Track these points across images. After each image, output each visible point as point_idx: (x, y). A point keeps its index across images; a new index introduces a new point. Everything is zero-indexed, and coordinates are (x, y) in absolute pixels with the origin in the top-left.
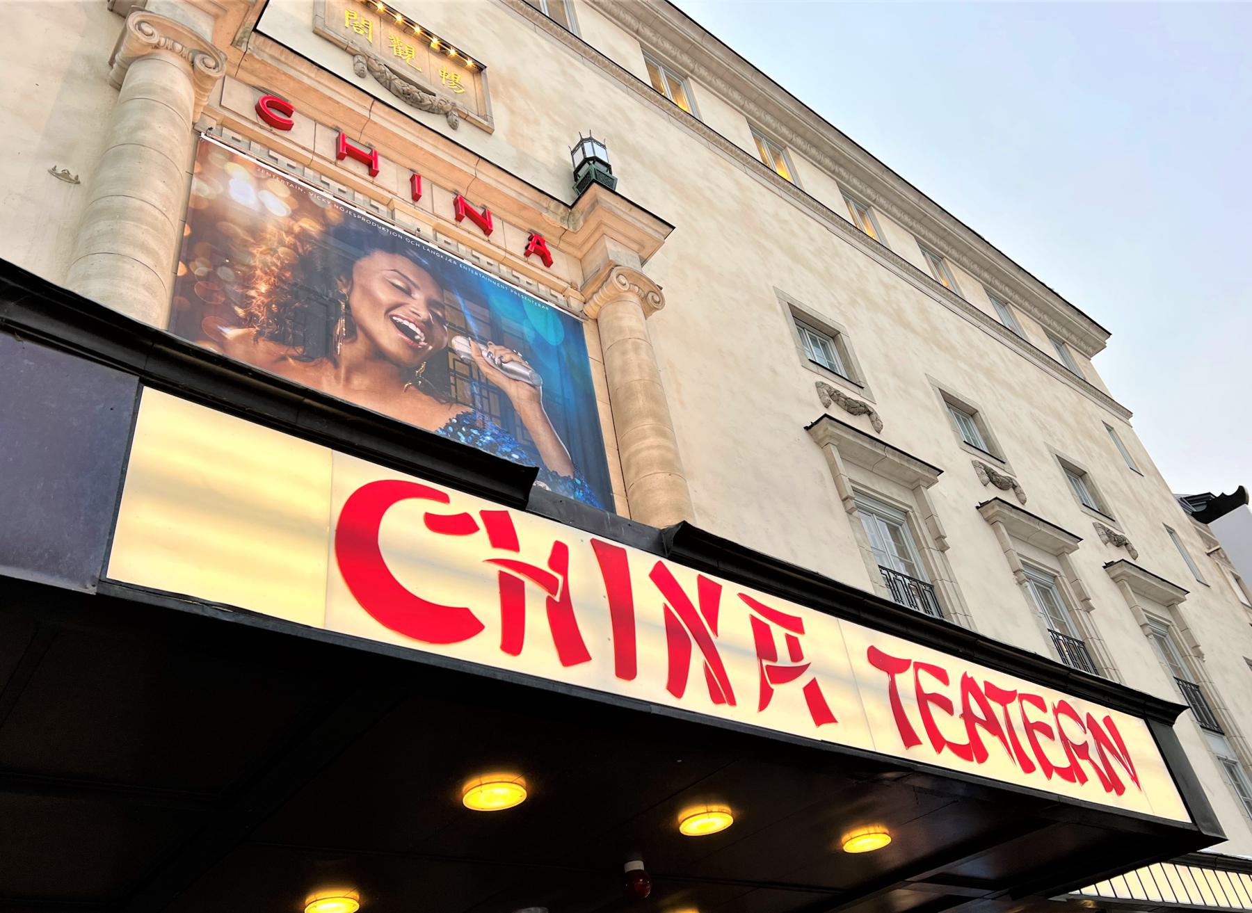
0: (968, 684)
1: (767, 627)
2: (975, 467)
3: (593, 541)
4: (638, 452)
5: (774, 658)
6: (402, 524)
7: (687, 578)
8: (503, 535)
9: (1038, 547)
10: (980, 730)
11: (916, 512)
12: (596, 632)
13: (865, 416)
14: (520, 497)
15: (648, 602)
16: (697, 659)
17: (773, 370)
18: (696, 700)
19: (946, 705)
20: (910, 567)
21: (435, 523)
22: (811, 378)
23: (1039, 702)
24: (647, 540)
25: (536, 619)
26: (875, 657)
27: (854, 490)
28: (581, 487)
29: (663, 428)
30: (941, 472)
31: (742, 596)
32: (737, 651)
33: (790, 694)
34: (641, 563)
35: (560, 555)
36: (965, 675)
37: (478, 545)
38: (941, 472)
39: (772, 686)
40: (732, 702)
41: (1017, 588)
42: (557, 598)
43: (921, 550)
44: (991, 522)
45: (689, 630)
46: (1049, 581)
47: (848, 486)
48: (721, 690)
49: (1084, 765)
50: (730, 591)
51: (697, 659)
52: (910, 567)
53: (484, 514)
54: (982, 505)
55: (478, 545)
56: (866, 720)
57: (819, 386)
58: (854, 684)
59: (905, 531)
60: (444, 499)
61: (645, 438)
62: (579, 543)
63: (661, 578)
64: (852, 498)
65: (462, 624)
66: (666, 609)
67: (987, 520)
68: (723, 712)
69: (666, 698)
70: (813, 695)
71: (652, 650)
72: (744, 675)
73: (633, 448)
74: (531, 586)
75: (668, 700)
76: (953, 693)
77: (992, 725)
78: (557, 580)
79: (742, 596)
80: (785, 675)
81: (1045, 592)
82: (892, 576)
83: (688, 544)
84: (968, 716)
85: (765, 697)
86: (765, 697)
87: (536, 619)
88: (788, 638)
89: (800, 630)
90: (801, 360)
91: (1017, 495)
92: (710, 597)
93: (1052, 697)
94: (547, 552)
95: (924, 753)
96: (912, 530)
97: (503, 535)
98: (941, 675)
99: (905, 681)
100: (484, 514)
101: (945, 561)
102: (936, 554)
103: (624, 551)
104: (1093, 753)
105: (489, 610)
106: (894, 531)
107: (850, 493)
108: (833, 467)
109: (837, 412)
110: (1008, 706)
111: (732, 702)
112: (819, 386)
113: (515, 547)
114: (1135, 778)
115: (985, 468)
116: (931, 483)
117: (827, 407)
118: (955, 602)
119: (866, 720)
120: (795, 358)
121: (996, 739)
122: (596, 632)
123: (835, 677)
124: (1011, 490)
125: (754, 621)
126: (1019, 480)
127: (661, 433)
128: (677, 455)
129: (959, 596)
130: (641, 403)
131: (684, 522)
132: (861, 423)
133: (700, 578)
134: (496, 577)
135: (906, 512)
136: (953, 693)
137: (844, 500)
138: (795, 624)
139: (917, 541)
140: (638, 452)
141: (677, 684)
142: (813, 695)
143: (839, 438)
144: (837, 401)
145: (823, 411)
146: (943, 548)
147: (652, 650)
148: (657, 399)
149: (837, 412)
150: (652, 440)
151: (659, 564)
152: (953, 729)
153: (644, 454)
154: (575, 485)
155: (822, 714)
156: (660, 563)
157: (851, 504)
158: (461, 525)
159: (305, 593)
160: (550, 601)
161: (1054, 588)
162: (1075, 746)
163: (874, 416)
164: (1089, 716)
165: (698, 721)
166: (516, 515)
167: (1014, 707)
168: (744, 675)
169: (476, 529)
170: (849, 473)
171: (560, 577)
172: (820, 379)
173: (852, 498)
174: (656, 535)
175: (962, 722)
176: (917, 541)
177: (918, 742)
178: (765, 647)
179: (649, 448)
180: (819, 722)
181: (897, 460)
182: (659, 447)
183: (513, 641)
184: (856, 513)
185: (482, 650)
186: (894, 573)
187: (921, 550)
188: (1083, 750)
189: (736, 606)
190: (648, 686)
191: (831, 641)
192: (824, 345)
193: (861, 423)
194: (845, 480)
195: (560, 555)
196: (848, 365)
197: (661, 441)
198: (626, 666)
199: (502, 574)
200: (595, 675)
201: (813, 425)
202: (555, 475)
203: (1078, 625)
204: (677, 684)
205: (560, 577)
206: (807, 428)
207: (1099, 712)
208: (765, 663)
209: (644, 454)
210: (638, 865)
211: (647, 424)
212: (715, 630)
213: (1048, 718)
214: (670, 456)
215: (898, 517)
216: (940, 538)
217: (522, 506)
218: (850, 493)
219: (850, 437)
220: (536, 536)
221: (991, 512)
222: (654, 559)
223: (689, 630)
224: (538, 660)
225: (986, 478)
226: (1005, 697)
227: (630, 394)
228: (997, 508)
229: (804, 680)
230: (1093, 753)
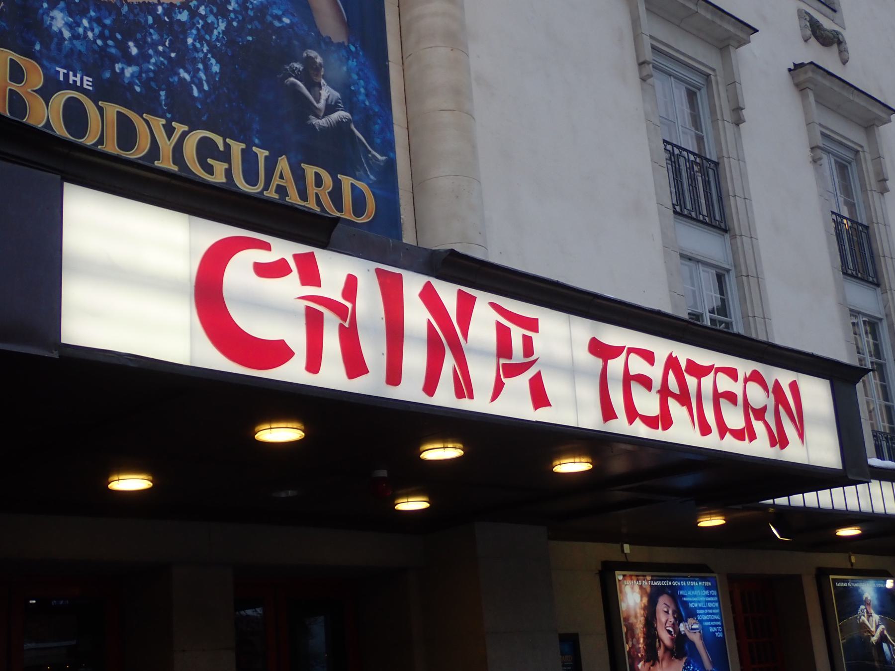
0: (672, 363)
2: (800, 17)
3: (378, 271)
5: (509, 355)
6: (239, 273)
7: (448, 294)
9: (847, 117)
10: (673, 404)
11: (719, 79)
12: (374, 351)
15: (416, 317)
19: (646, 382)
20: (700, 139)
21: (263, 270)
23: (732, 373)
25: (331, 343)
28: (355, 55)
30: (756, 31)
31: (494, 306)
32: (481, 353)
33: (520, 384)
36: (671, 354)
37: (290, 287)
38: (756, 31)
39: (504, 380)
40: (471, 397)
41: (810, 167)
42: (347, 325)
43: (714, 121)
44: (801, 88)
45: (445, 341)
46: (849, 155)
47: (647, 42)
48: (464, 388)
49: (758, 426)
51: (449, 363)
52: (700, 139)
53: (296, 257)
54: (797, 66)
56: (576, 404)
58: (572, 371)
59: (702, 98)
60: (267, 247)
62: (365, 272)
63: (429, 297)
65: (279, 352)
66: (429, 324)
67: (797, 85)
68: (465, 405)
69: (422, 398)
71: (415, 360)
72: (483, 373)
74: (328, 314)
76: (655, 373)
77: (683, 398)
80: (513, 370)
81: (843, 168)
82: (677, 151)
84: (665, 393)
86: (499, 387)
87: (331, 343)
88: (525, 337)
89: (536, 330)
91: (840, 52)
92: (466, 305)
93: (744, 367)
95: (620, 426)
96: (711, 97)
97: (310, 275)
98: (649, 357)
99: (616, 366)
100: (296, 257)
101: (738, 137)
102: (730, 127)
104: (770, 417)
106: (692, 96)
108: (635, 22)
110: (702, 379)
113: (318, 284)
114: (801, 436)
115: (811, 17)
116: (742, 43)
118: (737, 184)
119: (576, 404)
121: (685, 409)
122: (374, 351)
124: (835, 47)
125: (499, 325)
126: (848, 36)
129: (743, 175)
134: (303, 311)
135: (708, 76)
136: (655, 373)
137: (642, 64)
139: (713, 112)
141: (430, 387)
146: (738, 121)
147: (415, 360)
152: (647, 403)
154: (349, 51)
155: (540, 398)
157: (649, 69)
158: (277, 270)
159: (174, 338)
160: (341, 327)
161: (854, 164)
162: (754, 410)
164: (777, 383)
167: (707, 382)
168: (483, 373)
169: (289, 271)
170: (653, 28)
171: (349, 305)
175: (658, 396)
176: (713, 112)
177: (615, 417)
180: (536, 407)
181: (709, 16)
183: (314, 364)
185: (293, 372)
186: (679, 148)
187: (714, 121)
188: (760, 414)
191: (560, 336)
195: (350, 288)
198: (394, 376)
202: (328, 42)
203: (868, 207)
204: (430, 387)
205: (349, 305)
207: (785, 377)
208: (503, 361)
210: (383, 473)
212: (465, 336)
213: (736, 388)
215: (697, 80)
216: (737, 110)
220: (334, 269)
221: (802, 77)
225: (809, 32)
226: (699, 371)
228: (810, 74)
230: (770, 417)
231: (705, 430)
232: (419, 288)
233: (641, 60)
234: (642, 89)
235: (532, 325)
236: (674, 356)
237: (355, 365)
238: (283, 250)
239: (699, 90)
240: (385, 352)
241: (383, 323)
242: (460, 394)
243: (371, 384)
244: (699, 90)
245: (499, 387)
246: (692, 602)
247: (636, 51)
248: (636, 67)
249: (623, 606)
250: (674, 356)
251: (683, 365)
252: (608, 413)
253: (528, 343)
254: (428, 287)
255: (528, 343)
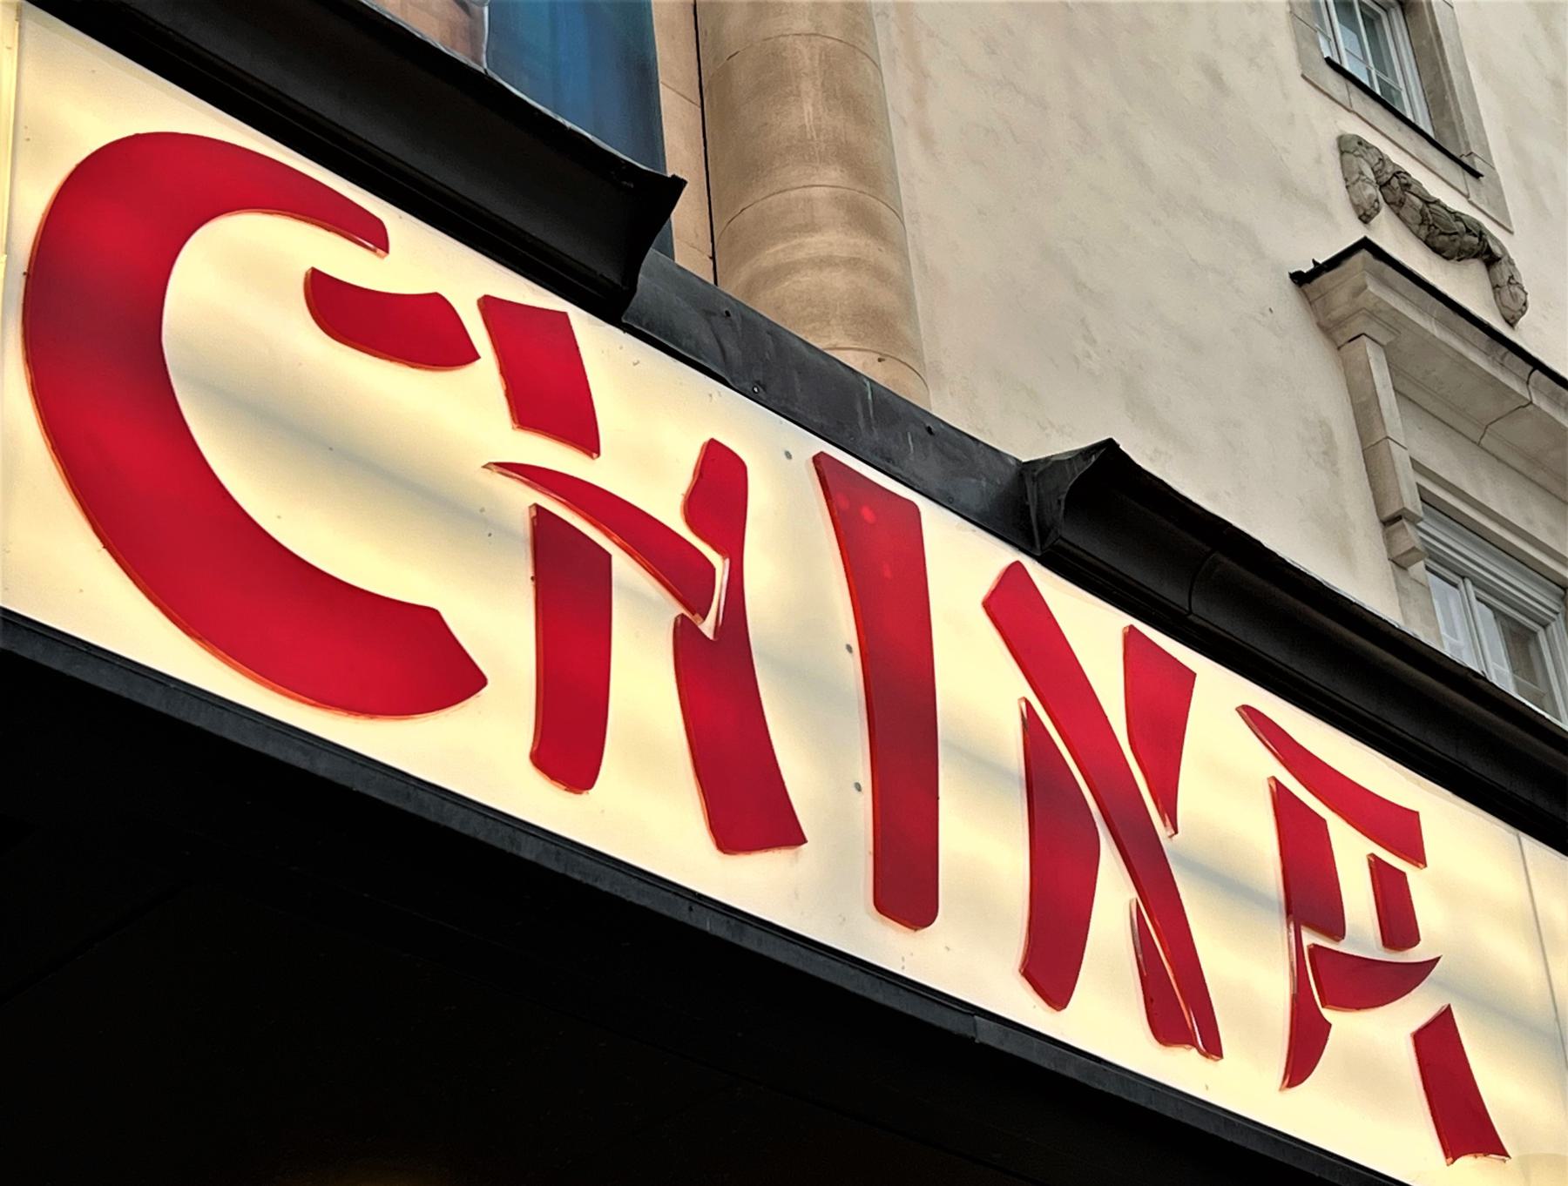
1: (1322, 822)
3: (819, 461)
4: (791, 268)
5: (1334, 925)
6: (236, 287)
7: (1094, 630)
8: (550, 396)
12: (821, 761)
13: (1476, 267)
14: (610, 273)
15: (979, 688)
16: (1114, 897)
17: (1214, 76)
18: (1104, 1020)
21: (333, 305)
22: (1334, 119)
24: (974, 491)
27: (1426, 498)
29: (872, 208)
31: (1251, 716)
33: (1376, 1037)
34: (962, 562)
35: (719, 485)
39: (1328, 1014)
40: (1213, 1048)
42: (707, 627)
45: (1095, 798)
48: (1178, 1002)
50: (1218, 694)
51: (1114, 897)
53: (490, 307)
55: (463, 414)
57: (1348, 147)
60: (374, 236)
61: (811, 227)
62: (780, 463)
63: (1016, 616)
64: (1414, 520)
65: (425, 664)
70: (1438, 1049)
71: (984, 842)
72: (1250, 970)
73: (769, 257)
74: (625, 570)
75: (1019, 1004)
78: (711, 569)
79: (1251, 716)
83: (1098, 515)
85: (1304, 1052)
86: (1304, 1052)
88: (1378, 868)
89: (1417, 856)
90: (1302, 57)
92: (1161, 709)
94: (683, 479)
97: (550, 396)
100: (490, 307)
105: (498, 625)
107: (1413, 503)
109: (1391, 235)
111: (1213, 1048)
112: (1348, 147)
113: (586, 439)
117: (1365, 218)
120: (1284, 47)
122: (821, 761)
123: (1506, 1013)
125: (1282, 800)
127: (864, 219)
128: (907, 297)
130: (807, 112)
131: (1110, 445)
132: (1464, 285)
133: (1131, 636)
134: (522, 526)
137: (1390, 522)
138: (1397, 831)
140: (791, 268)
141: (1053, 962)
142: (1438, 1049)
143: (1395, 323)
144: (1397, 206)
145: (1356, 232)
147: (984, 842)
148: (858, 104)
149: (1391, 235)
150: (832, 240)
151: (1015, 569)
153: (806, 280)
156: (1016, 567)
157: (1409, 537)
158: (414, 333)
160: (684, 635)
163: (1502, 270)
165: (1111, 1088)
166: (589, 331)
168: (1250, 970)
169: (470, 356)
170: (1412, 441)
172: (1354, 127)
173: (1414, 520)
174: (1006, 477)
178: (1309, 893)
179: (825, 262)
182: (853, 263)
183: (570, 739)
184: (1418, 569)
185: (475, 753)
189: (1230, 753)
190: (968, 956)
192: (1371, 21)
193: (1464, 285)
194: (1401, 457)
195: (719, 485)
196: (1439, 94)
197: (861, 244)
198: (906, 880)
199: (541, 517)
200: (807, 892)
201: (1319, 269)
206: (1299, 279)
208: (1309, 938)
209: (806, 280)
211: (825, 183)
212: (1169, 809)
214: (885, 298)
217: (611, 306)
218: (1413, 503)
219: (1428, 323)
220: (652, 421)
222: (1003, 555)
223: (1095, 798)
224: (643, 815)
227: (775, 76)
229: (1414, 1010)
232: (986, 581)
233: (1389, 512)
234: (1400, 589)
239: (1545, 626)
240: (864, 775)
241: (851, 669)
244: (1545, 626)
247: (1370, 477)
248: (1377, 530)
254: (1013, 577)
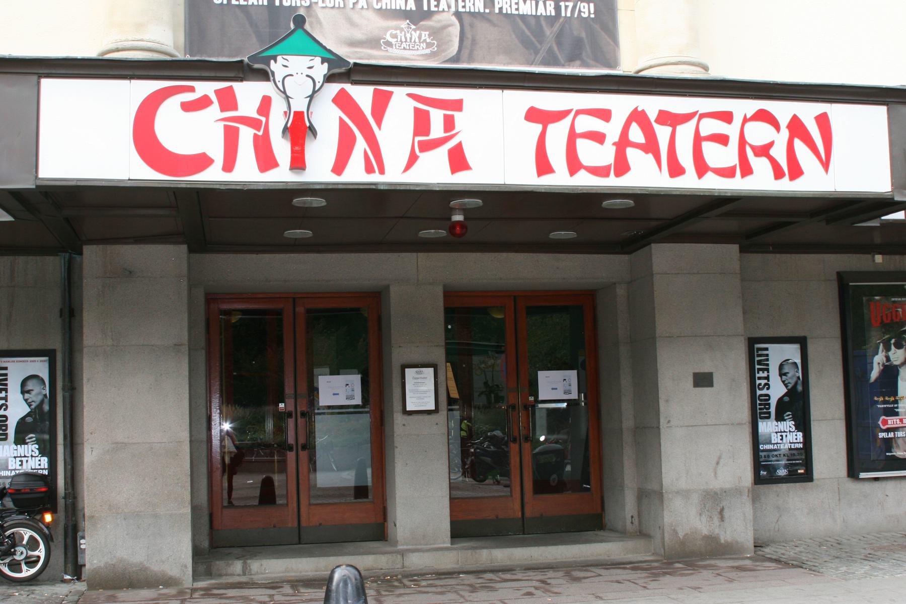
0: (638, 116)
10: (632, 154)
21: (187, 107)
26: (533, 115)
31: (409, 95)
37: (214, 111)
53: (217, 92)
55: (214, 111)
60: (192, 89)
65: (203, 161)
78: (261, 121)
79: (409, 95)
86: (413, 159)
97: (228, 101)
100: (217, 92)
103: (427, 112)
105: (217, 153)
155: (458, 160)
158: (203, 103)
159: (126, 167)
162: (752, 147)
171: (263, 119)
185: (213, 175)
199: (226, 127)
205: (263, 119)
231: (676, 170)
235: (457, 105)
236: (639, 109)
237: (266, 160)
238: (206, 88)
242: (369, 169)
243: (282, 175)
245: (413, 159)
246: (379, 399)
249: (760, 431)
250: (639, 109)
251: (652, 116)
252: (544, 166)
253: (449, 124)
255: (449, 124)
